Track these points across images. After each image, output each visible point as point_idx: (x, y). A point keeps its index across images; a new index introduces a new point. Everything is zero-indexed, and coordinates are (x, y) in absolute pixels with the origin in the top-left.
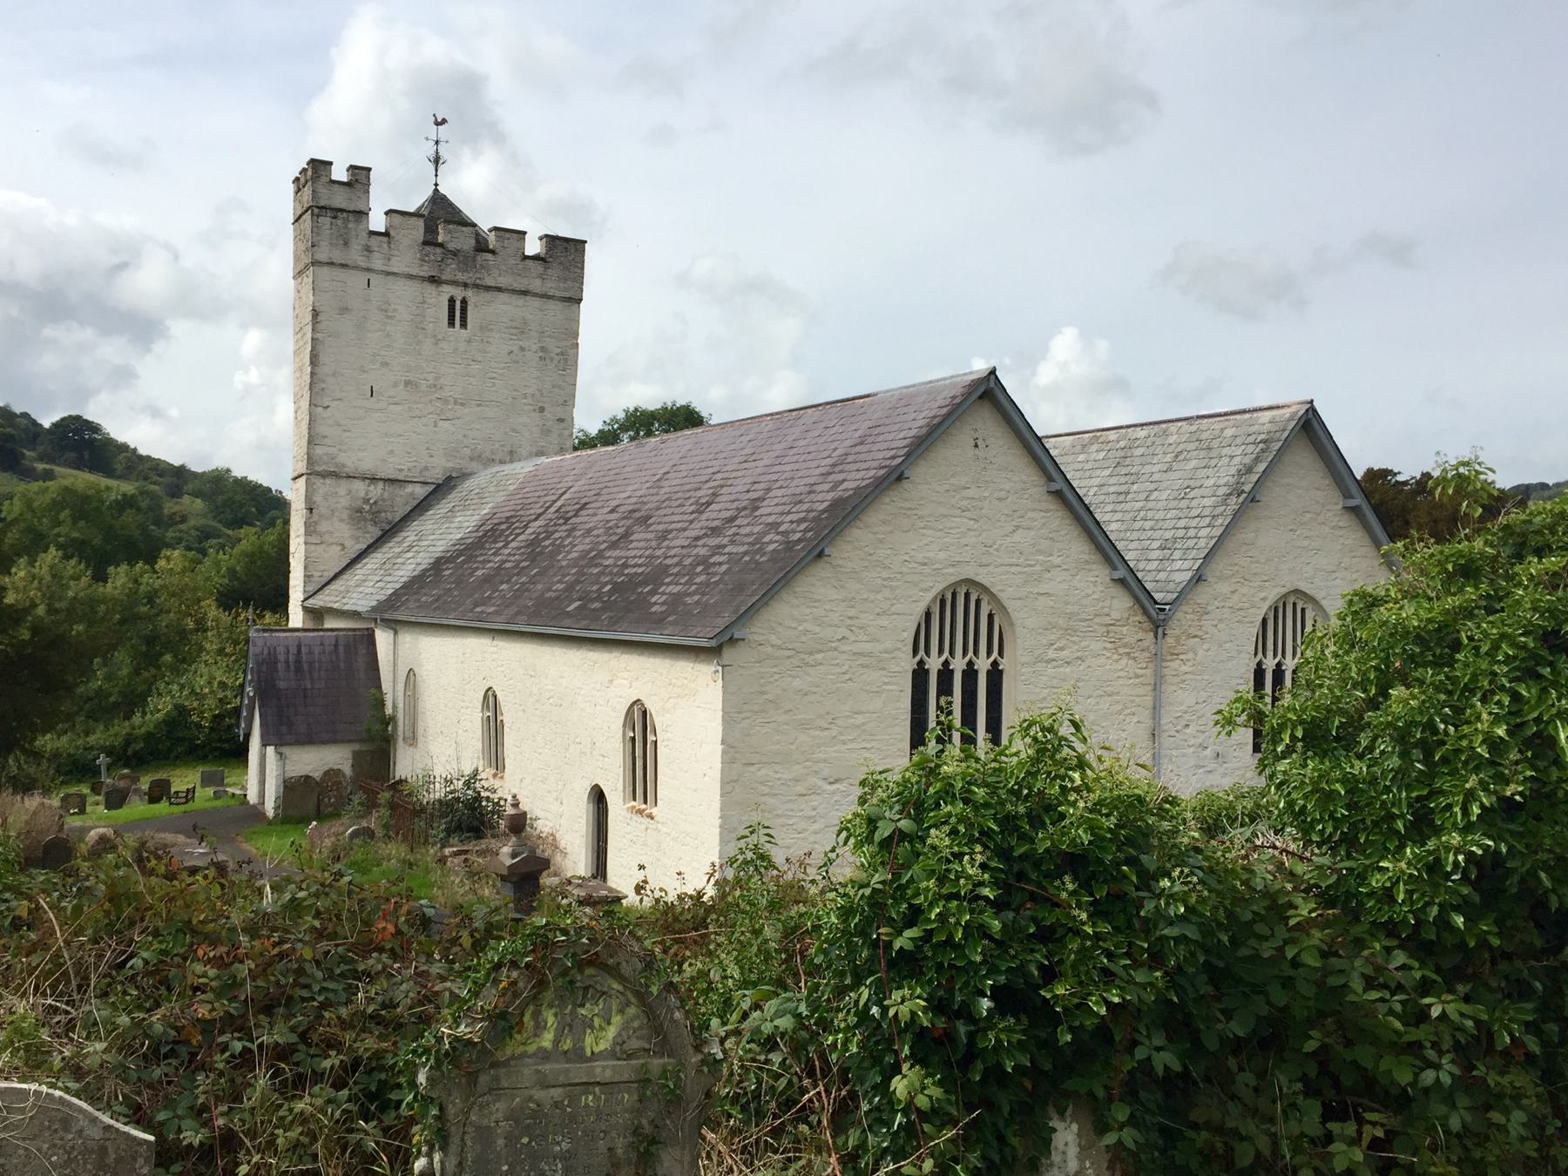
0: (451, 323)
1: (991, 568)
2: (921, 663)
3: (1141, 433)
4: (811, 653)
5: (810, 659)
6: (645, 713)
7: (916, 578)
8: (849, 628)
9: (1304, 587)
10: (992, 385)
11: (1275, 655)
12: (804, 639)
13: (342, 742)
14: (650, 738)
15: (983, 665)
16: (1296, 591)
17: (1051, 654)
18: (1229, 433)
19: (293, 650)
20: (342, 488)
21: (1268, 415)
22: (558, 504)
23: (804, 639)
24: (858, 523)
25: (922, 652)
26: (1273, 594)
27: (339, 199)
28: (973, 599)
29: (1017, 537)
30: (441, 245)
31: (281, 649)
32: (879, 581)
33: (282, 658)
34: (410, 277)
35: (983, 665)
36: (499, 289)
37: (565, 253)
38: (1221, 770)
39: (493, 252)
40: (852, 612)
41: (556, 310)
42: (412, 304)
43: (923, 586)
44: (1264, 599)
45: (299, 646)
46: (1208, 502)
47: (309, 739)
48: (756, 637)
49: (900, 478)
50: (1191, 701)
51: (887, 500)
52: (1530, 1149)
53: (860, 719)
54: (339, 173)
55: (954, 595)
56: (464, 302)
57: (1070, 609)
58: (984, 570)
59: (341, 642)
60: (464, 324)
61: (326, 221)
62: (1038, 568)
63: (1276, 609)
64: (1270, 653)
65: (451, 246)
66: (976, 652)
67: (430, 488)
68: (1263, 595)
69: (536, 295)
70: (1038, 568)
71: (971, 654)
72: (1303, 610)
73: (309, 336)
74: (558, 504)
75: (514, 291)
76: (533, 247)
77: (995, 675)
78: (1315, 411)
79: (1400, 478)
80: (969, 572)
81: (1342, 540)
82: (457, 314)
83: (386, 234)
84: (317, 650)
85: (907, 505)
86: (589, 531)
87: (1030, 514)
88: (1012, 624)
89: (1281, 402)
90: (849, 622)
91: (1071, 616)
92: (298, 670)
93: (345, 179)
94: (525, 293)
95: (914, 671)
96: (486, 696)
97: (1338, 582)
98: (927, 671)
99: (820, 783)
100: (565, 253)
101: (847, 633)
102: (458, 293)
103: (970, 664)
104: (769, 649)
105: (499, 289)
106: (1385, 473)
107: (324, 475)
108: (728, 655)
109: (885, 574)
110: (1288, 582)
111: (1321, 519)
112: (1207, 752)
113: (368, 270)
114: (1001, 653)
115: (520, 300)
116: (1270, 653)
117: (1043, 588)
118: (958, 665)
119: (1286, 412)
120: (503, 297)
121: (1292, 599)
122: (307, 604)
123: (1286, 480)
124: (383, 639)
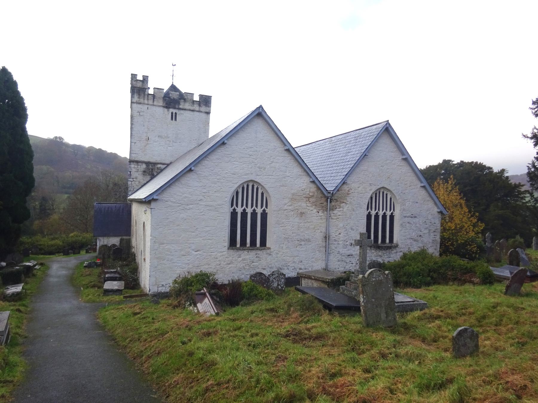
0: (172, 119)
1: (261, 176)
2: (234, 210)
3: (341, 137)
4: (188, 205)
5: (186, 207)
8: (203, 196)
9: (385, 186)
10: (261, 110)
11: (375, 210)
12: (185, 200)
16: (383, 188)
17: (286, 207)
21: (375, 127)
23: (185, 200)
24: (208, 159)
25: (235, 206)
26: (374, 189)
32: (216, 180)
34: (160, 106)
36: (185, 110)
37: (206, 101)
40: (205, 191)
41: (204, 115)
42: (161, 113)
48: (165, 199)
49: (224, 144)
51: (219, 151)
53: (208, 229)
54: (140, 78)
55: (248, 186)
56: (176, 113)
59: (121, 207)
60: (176, 120)
63: (376, 194)
64: (374, 209)
66: (257, 206)
69: (197, 111)
71: (254, 207)
72: (387, 194)
75: (190, 110)
76: (196, 98)
77: (264, 215)
78: (389, 124)
79: (454, 163)
82: (174, 117)
84: (114, 209)
85: (227, 153)
87: (278, 158)
88: (270, 197)
90: (204, 194)
93: (142, 79)
94: (193, 111)
95: (232, 212)
98: (247, 213)
99: (191, 251)
100: (206, 101)
101: (203, 198)
103: (244, 210)
104: (170, 203)
105: (185, 110)
106: (450, 161)
108: (153, 205)
109: (218, 177)
111: (393, 162)
112: (348, 243)
113: (148, 104)
114: (266, 207)
115: (192, 113)
116: (374, 209)
118: (249, 211)
120: (187, 112)
121: (382, 191)
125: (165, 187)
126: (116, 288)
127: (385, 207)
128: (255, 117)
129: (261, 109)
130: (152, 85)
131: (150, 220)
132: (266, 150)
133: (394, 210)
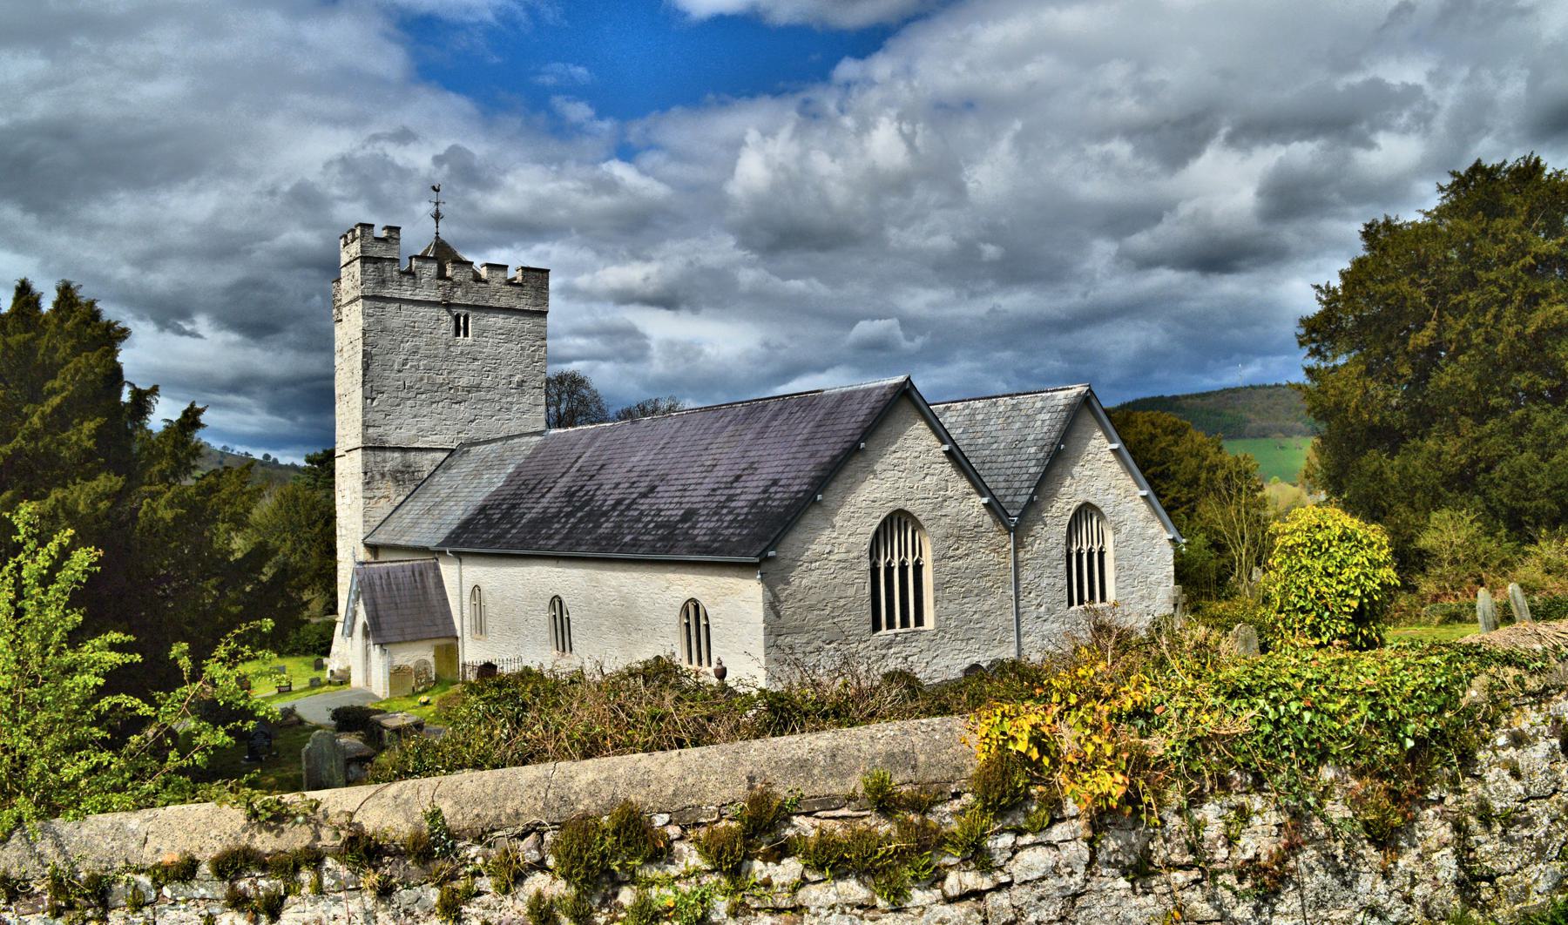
6: (697, 608)
13: (422, 640)
14: (703, 622)
15: (1096, 549)
17: (951, 553)
18: (1039, 405)
19: (385, 576)
22: (578, 465)
26: (1074, 506)
27: (377, 250)
29: (928, 480)
30: (449, 279)
31: (376, 576)
33: (378, 582)
35: (1096, 549)
39: (486, 282)
46: (1033, 450)
47: (405, 640)
52: (693, 880)
61: (370, 267)
65: (456, 279)
67: (445, 455)
73: (360, 348)
74: (578, 465)
80: (900, 504)
84: (400, 575)
86: (617, 485)
92: (390, 589)
96: (685, 608)
102: (463, 312)
107: (373, 449)
110: (1081, 499)
117: (943, 512)
118: (1085, 548)
122: (369, 540)
124: (450, 572)
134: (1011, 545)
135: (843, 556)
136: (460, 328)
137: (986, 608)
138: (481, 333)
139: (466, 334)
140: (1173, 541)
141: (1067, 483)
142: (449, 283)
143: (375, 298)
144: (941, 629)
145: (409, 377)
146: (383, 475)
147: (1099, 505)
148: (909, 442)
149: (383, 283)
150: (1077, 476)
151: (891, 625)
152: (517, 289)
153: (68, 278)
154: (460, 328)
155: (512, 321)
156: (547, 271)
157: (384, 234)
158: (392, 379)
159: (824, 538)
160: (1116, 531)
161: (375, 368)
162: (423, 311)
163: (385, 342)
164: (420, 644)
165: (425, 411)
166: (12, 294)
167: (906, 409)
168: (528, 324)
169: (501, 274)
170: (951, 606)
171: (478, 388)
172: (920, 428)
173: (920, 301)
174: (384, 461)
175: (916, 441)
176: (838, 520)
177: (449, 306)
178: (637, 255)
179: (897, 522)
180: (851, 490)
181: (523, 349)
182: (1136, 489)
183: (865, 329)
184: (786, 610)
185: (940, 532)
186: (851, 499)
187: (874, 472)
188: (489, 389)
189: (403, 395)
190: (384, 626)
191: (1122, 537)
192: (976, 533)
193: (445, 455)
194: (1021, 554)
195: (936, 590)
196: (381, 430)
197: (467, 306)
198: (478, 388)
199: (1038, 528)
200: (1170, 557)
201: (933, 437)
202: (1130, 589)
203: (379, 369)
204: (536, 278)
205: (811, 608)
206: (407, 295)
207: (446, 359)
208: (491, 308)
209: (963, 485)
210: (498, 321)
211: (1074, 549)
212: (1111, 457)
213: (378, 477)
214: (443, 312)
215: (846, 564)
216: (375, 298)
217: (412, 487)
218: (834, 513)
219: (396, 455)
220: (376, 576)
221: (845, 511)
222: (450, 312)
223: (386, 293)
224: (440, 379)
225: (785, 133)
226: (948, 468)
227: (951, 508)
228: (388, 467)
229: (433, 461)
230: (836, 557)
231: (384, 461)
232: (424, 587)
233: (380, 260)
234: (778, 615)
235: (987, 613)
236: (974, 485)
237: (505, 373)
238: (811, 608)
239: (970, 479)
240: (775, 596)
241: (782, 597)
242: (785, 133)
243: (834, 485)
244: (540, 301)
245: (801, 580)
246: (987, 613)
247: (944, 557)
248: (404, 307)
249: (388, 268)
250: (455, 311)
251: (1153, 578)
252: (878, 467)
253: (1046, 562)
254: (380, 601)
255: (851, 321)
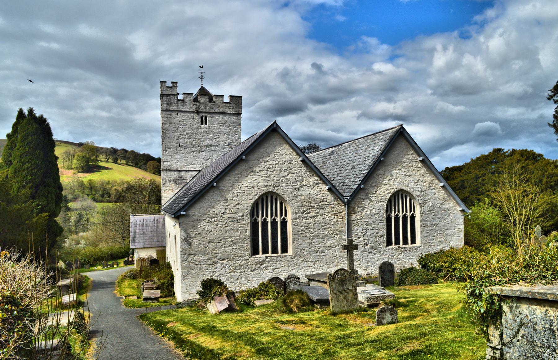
3: (363, 140)
7: (250, 192)
17: (304, 215)
19: (142, 221)
20: (190, 173)
26: (392, 191)
27: (168, 92)
28: (274, 198)
33: (138, 223)
38: (374, 252)
43: (253, 194)
44: (389, 193)
45: (143, 220)
50: (361, 229)
54: (169, 84)
57: (310, 199)
58: (276, 188)
61: (165, 98)
62: (298, 186)
64: (393, 212)
67: (197, 173)
68: (388, 192)
70: (298, 186)
76: (226, 99)
79: (505, 151)
80: (271, 189)
81: (419, 172)
83: (183, 100)
89: (394, 126)
91: (311, 202)
97: (418, 186)
102: (204, 115)
110: (397, 187)
111: (410, 165)
116: (393, 212)
117: (300, 193)
119: (395, 129)
123: (396, 152)
125: (228, 169)
126: (153, 296)
127: (404, 209)
128: (269, 133)
129: (275, 126)
130: (181, 90)
131: (179, 234)
132: (282, 163)
133: (414, 211)
134: (345, 212)
135: (233, 215)
136: (203, 121)
137: (328, 245)
138: (213, 123)
139: (206, 124)
140: (463, 211)
141: (388, 178)
142: (198, 104)
143: (167, 110)
144: (295, 255)
145: (181, 142)
146: (170, 181)
147: (410, 191)
148: (277, 156)
149: (170, 104)
150: (395, 175)
151: (265, 251)
152: (228, 105)
153: (32, 107)
154: (203, 121)
155: (226, 118)
156: (223, 96)
157: (171, 85)
158: (174, 143)
159: (220, 206)
160: (422, 205)
161: (167, 138)
162: (187, 115)
163: (171, 128)
164: (151, 249)
165: (188, 155)
166: (17, 113)
167: (275, 140)
168: (232, 119)
169: (221, 99)
170: (304, 243)
171: (211, 146)
172: (286, 148)
173: (512, 112)
174: (171, 175)
175: (283, 155)
176: (229, 197)
177: (198, 112)
178: (389, 100)
179: (268, 199)
180: (238, 181)
181: (230, 129)
182: (438, 182)
183: (481, 126)
184: (195, 242)
185: (297, 204)
186: (238, 185)
187: (253, 172)
188: (216, 146)
189: (179, 149)
190: (137, 241)
191: (426, 208)
192: (322, 204)
193: (197, 173)
194: (353, 217)
195: (293, 234)
196: (170, 163)
197: (206, 113)
198: (211, 146)
199: (366, 203)
200: (461, 221)
201: (294, 154)
202: (431, 237)
203: (169, 139)
204: (236, 100)
205: (210, 242)
206: (181, 109)
207: (197, 134)
208: (216, 113)
209: (314, 179)
210: (220, 118)
211: (393, 215)
212: (420, 165)
213: (168, 182)
214: (195, 115)
215: (234, 220)
216: (167, 110)
217: (182, 186)
218: (227, 192)
219: (176, 173)
220: (138, 221)
221: (235, 191)
222: (198, 115)
223: (171, 108)
224: (194, 142)
225: (451, 48)
226: (304, 170)
227: (305, 191)
228: (172, 177)
229: (191, 175)
230: (228, 216)
231: (171, 175)
232: (157, 226)
233: (169, 95)
234: (190, 244)
235: (329, 248)
236: (321, 179)
237: (223, 139)
238: (210, 242)
239: (318, 176)
240: (188, 235)
241: (193, 235)
242: (451, 48)
243: (227, 178)
244: (238, 109)
245: (204, 227)
246: (329, 248)
247: (299, 217)
248: (179, 114)
249: (172, 99)
250: (201, 115)
251: (448, 232)
252: (257, 169)
253: (371, 221)
254: (137, 231)
255: (474, 122)
